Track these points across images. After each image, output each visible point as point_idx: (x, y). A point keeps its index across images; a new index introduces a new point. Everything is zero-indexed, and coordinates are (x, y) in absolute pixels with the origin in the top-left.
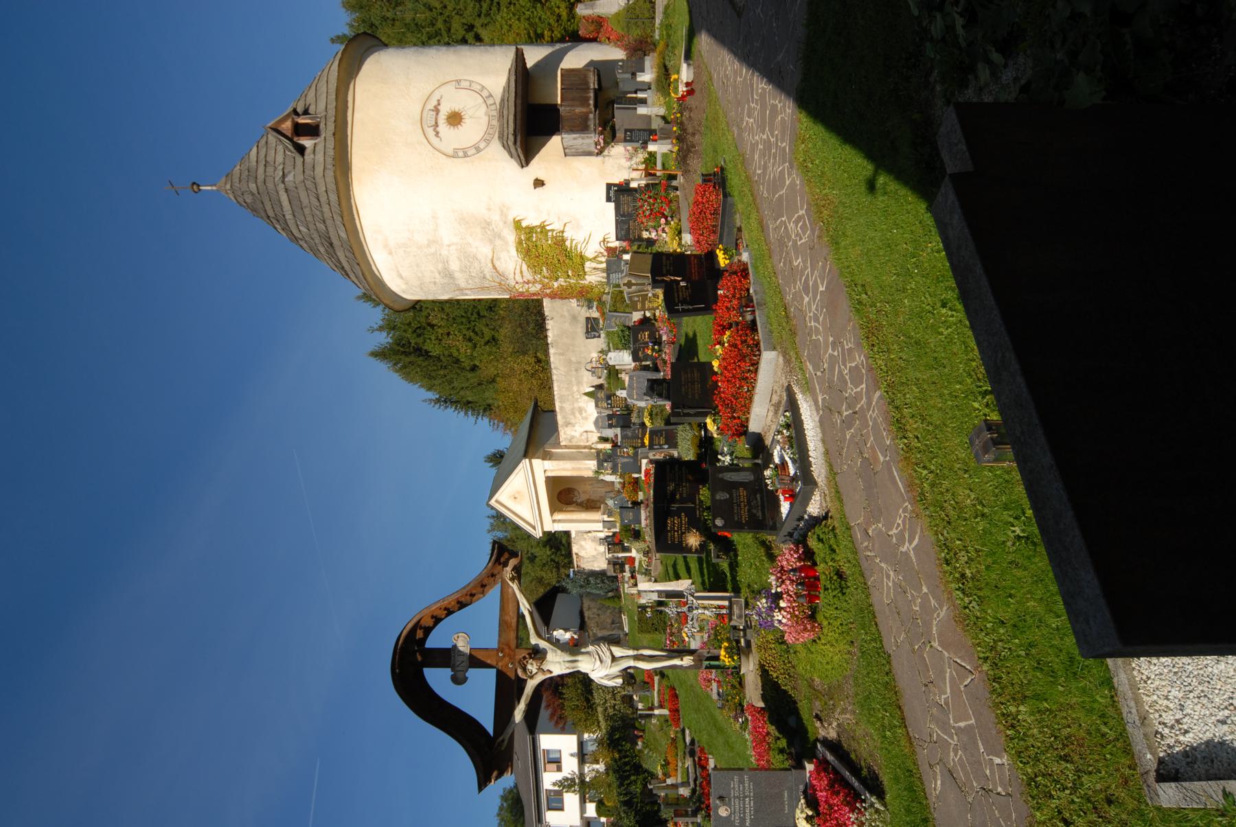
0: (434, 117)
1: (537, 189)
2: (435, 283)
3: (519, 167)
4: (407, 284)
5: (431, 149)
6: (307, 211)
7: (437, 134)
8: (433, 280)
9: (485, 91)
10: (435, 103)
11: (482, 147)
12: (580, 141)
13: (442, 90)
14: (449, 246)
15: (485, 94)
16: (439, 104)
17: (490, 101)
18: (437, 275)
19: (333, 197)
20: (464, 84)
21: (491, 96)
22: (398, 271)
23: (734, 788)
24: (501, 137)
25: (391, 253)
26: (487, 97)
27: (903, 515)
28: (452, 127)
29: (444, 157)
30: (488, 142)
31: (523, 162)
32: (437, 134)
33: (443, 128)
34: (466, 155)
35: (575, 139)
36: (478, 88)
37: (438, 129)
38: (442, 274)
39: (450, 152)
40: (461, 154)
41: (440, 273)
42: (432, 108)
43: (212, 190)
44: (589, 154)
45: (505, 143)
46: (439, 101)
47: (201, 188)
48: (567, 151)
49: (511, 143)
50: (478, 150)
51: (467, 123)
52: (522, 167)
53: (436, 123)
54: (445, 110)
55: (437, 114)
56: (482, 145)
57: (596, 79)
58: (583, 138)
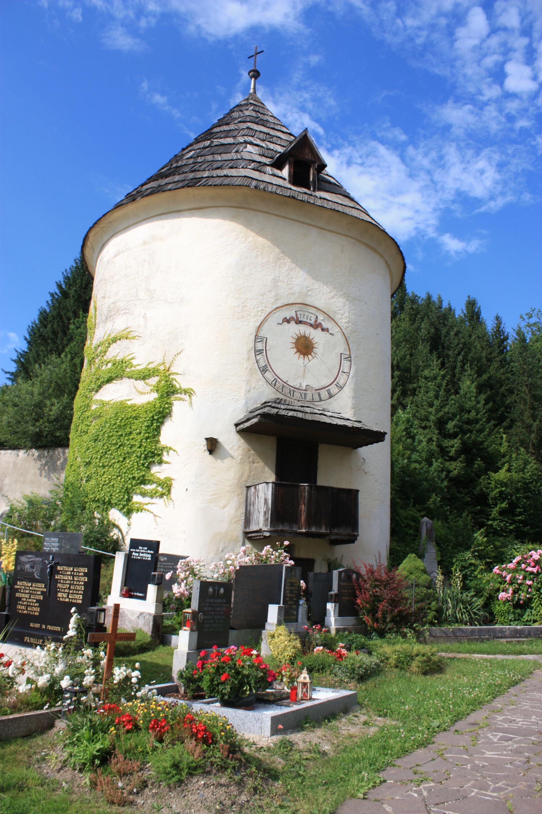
0: (309, 321)
1: (205, 442)
2: (104, 297)
3: (236, 421)
4: (108, 262)
5: (269, 310)
6: (210, 158)
7: (288, 321)
8: (107, 295)
9: (337, 390)
10: (325, 325)
11: (268, 375)
12: (262, 509)
13: (339, 337)
14: (144, 317)
15: (334, 389)
16: (323, 330)
17: (324, 394)
18: (112, 300)
19: (218, 181)
20: (346, 364)
21: (331, 396)
22: (123, 252)
23: (31, 586)
24: (278, 401)
25: (145, 243)
26: (329, 391)
27: (405, 521)
28: (294, 341)
29: (258, 324)
30: (273, 384)
31: (242, 426)
32: (288, 321)
33: (294, 330)
34: (258, 352)
35: (266, 500)
36: (342, 380)
37: (293, 323)
38: (112, 306)
39: (262, 334)
40: (260, 346)
41: (114, 303)
42: (319, 321)
43: (250, 89)
44: (247, 521)
45: (270, 404)
46: (327, 330)
47: (253, 79)
48: (253, 489)
49: (266, 410)
50: (264, 370)
51: (299, 361)
52: (237, 425)
53: (301, 322)
54: (316, 335)
55: (311, 325)
56: (269, 375)
57: (343, 537)
58: (265, 513)
